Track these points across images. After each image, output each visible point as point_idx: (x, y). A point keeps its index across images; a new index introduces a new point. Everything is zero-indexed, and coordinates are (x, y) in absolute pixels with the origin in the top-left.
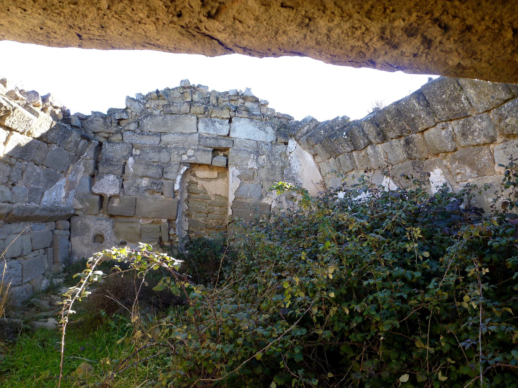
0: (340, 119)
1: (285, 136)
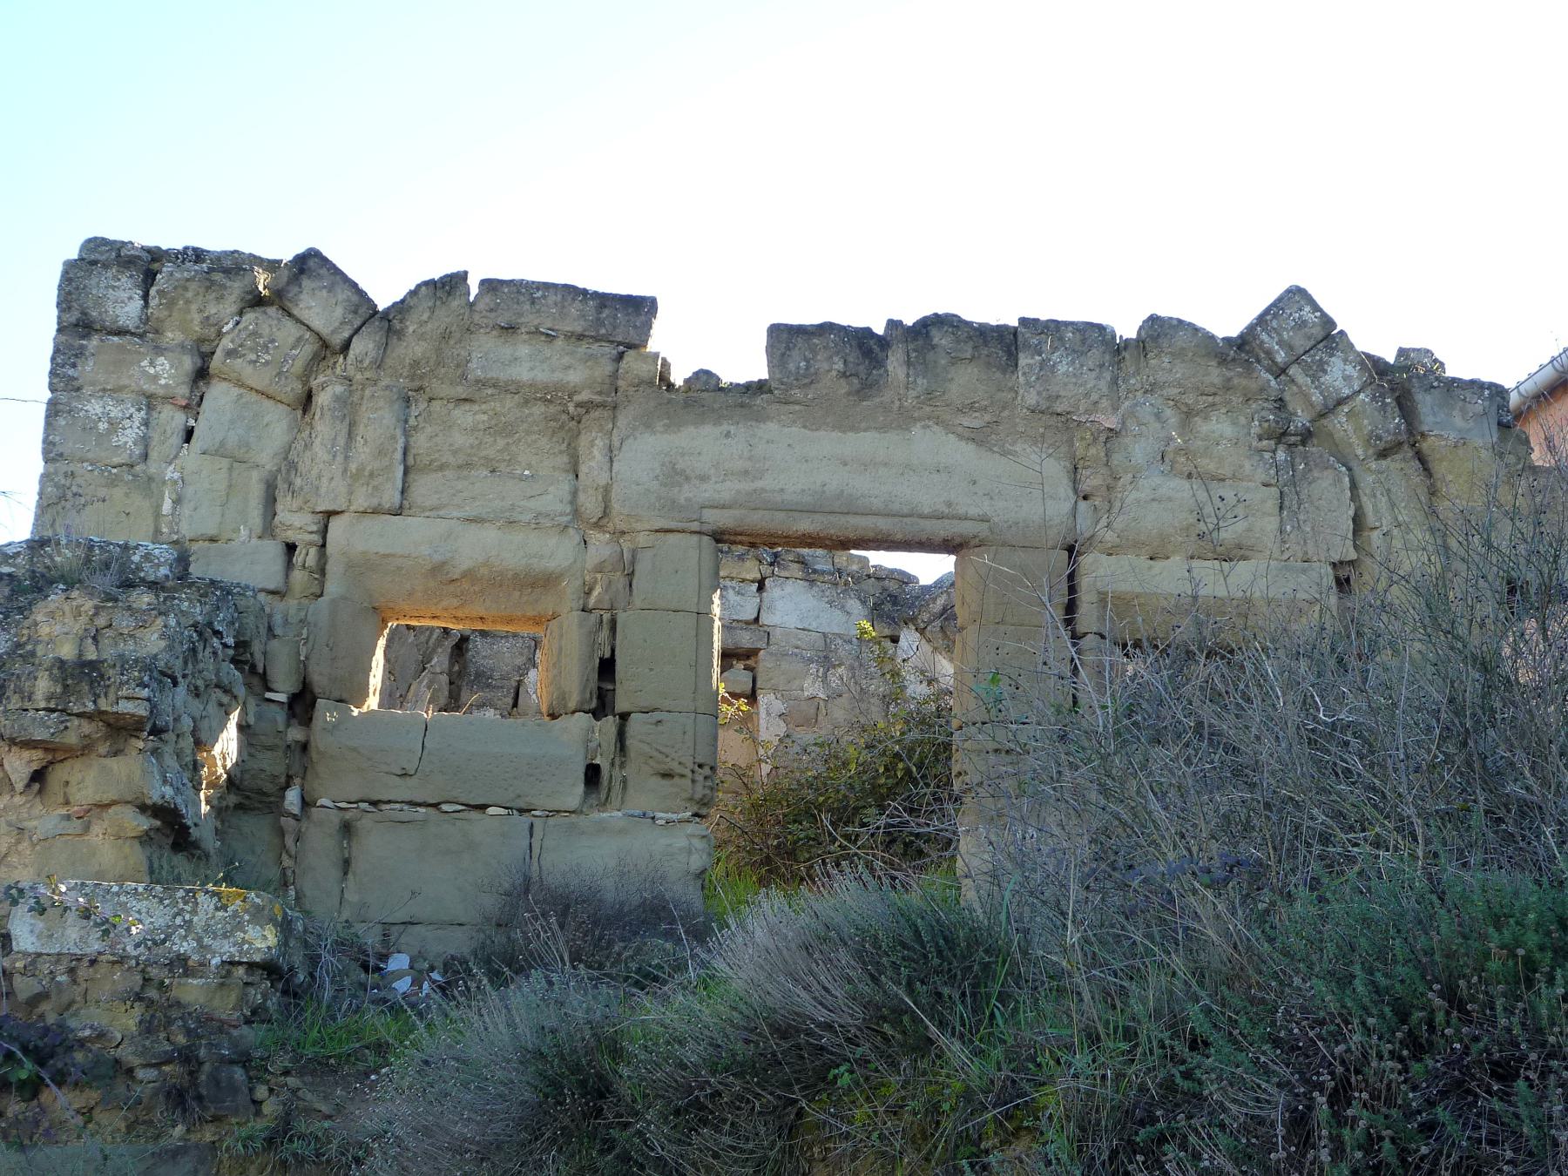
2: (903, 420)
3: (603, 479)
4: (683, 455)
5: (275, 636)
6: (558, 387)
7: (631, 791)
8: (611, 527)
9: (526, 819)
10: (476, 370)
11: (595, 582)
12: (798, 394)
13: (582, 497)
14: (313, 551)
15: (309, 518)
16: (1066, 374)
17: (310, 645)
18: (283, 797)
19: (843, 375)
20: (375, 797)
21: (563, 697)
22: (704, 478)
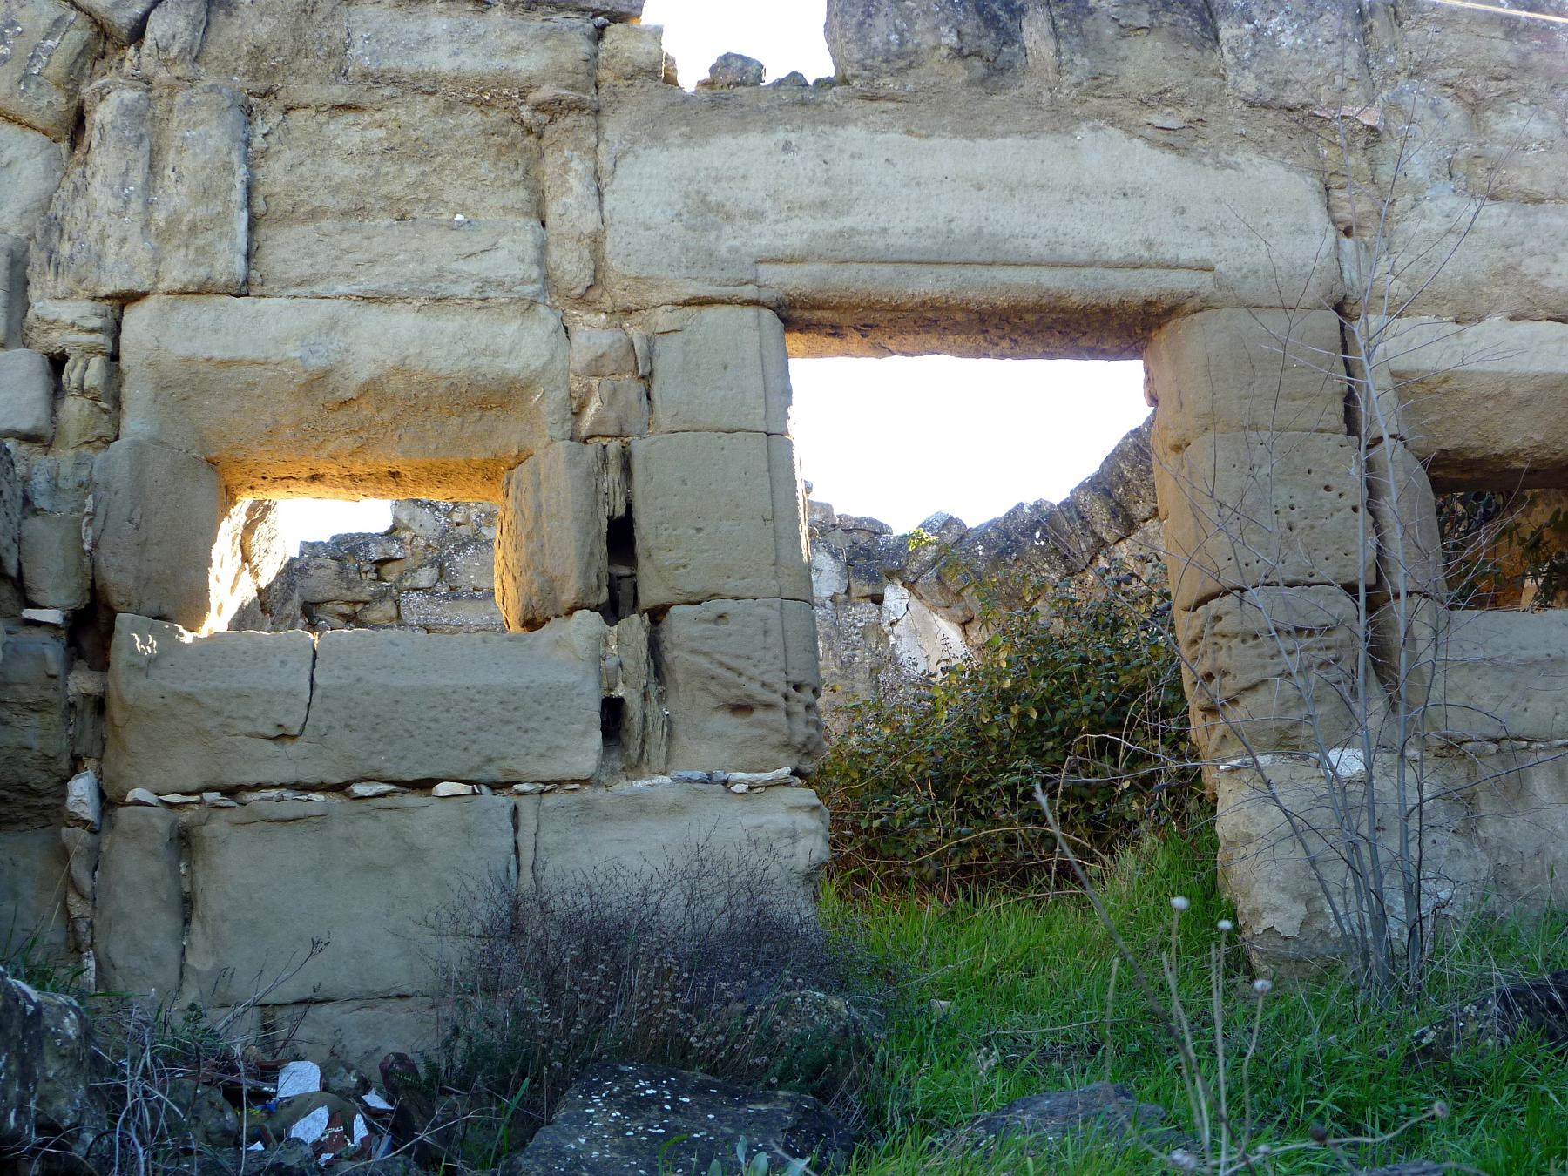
0: (1026, 510)
1: (873, 578)
2: (1060, 119)
3: (589, 223)
4: (717, 180)
5: (36, 512)
6: (502, 80)
7: (682, 739)
8: (607, 303)
9: (503, 800)
10: (362, 57)
11: (589, 393)
12: (890, 84)
13: (555, 255)
14: (96, 363)
15: (86, 307)
16: (1294, 48)
17: (99, 522)
18: (64, 796)
19: (958, 54)
20: (233, 778)
21: (550, 588)
22: (755, 215)
